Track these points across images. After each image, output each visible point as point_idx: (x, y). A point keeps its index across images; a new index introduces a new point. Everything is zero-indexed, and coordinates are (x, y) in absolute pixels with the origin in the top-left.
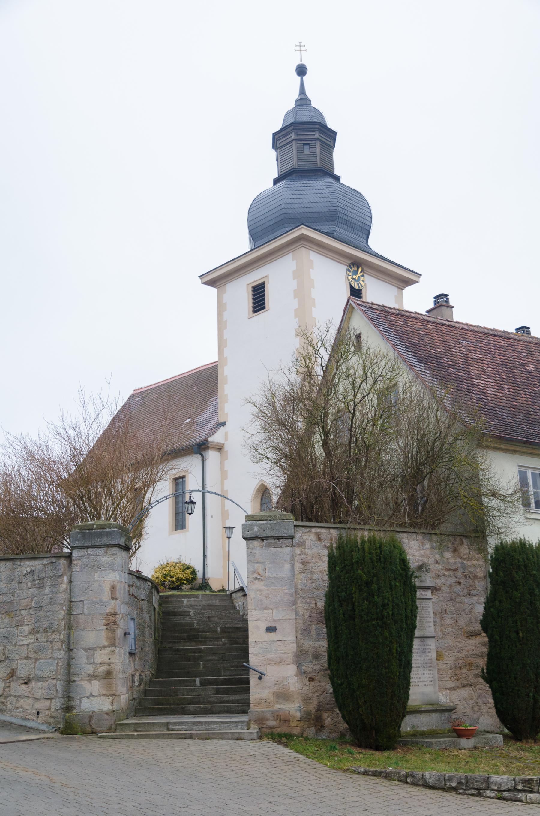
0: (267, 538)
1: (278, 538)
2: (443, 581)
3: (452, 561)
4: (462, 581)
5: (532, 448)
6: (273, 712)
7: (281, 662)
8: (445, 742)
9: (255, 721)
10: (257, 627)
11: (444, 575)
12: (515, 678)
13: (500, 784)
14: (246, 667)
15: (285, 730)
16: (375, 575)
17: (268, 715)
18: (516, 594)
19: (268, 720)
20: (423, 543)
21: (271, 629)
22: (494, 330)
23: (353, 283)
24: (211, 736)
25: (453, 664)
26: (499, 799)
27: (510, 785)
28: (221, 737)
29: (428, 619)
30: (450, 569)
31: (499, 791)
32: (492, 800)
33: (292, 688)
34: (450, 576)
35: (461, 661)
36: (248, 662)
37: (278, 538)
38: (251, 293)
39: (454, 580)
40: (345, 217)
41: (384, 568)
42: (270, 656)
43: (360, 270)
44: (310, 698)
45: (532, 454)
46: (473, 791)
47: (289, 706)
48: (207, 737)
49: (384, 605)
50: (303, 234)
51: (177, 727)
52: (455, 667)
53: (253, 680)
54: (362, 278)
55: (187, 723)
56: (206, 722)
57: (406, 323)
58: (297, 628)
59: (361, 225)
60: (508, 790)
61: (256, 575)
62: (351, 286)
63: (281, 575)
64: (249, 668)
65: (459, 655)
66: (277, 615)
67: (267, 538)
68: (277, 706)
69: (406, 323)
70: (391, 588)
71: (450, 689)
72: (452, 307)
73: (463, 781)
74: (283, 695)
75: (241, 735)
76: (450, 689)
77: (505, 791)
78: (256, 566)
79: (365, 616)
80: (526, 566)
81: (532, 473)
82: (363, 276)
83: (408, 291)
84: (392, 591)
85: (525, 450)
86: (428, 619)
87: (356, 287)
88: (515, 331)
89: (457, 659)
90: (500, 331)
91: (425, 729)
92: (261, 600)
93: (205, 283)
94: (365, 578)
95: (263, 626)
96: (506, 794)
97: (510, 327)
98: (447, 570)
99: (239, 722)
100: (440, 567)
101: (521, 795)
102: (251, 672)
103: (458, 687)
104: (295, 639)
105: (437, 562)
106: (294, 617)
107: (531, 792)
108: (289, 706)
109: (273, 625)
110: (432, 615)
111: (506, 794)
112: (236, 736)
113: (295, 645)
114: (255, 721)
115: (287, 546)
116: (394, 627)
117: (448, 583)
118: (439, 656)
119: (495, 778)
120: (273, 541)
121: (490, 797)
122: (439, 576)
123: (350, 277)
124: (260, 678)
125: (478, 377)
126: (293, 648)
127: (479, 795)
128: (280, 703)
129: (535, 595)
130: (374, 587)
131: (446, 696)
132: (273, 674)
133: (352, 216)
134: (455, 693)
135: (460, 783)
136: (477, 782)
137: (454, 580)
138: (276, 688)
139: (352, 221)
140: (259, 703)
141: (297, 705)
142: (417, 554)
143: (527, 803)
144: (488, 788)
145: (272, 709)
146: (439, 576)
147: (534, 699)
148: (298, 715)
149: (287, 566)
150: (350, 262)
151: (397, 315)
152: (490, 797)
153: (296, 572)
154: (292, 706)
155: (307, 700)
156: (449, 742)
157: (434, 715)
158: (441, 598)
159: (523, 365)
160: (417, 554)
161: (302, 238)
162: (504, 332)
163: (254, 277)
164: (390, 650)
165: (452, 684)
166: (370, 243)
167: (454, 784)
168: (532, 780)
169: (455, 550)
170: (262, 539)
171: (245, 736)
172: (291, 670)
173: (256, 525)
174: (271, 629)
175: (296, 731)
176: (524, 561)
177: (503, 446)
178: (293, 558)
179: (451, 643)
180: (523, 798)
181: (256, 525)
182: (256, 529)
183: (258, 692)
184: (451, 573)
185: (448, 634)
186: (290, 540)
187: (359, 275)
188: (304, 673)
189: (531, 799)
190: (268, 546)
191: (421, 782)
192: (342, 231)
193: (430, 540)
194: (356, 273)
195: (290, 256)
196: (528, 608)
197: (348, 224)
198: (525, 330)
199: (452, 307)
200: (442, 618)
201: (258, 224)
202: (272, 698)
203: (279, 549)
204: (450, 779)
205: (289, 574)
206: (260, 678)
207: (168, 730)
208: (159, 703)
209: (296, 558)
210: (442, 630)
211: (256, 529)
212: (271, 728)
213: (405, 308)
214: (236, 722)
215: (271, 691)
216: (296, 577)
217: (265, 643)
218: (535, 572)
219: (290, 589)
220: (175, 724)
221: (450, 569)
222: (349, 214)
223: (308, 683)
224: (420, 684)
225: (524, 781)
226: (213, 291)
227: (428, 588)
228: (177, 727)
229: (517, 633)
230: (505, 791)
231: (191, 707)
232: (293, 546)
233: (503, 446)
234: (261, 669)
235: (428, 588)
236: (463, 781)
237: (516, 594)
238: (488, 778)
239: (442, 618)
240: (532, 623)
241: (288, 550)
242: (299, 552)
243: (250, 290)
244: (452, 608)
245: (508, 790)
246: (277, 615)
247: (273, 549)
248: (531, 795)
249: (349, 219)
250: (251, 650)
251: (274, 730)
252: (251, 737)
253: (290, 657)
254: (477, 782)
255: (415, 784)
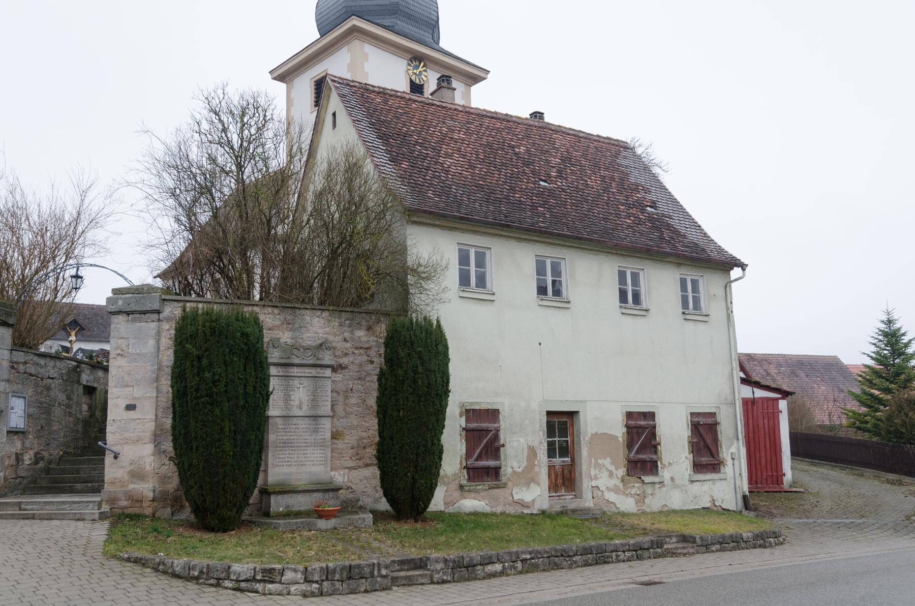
0: (132, 312)
1: (144, 313)
2: (351, 359)
3: (365, 339)
4: (375, 360)
5: (473, 226)
6: (125, 493)
7: (138, 441)
8: (297, 523)
9: (107, 501)
10: (117, 405)
11: (353, 353)
12: (395, 458)
13: (239, 574)
14: (102, 447)
15: (136, 510)
16: (206, 350)
17: (120, 495)
18: (400, 372)
19: (120, 500)
20: (329, 321)
21: (130, 407)
22: (496, 113)
23: (413, 78)
24: (53, 516)
25: (355, 444)
26: (235, 589)
27: (249, 574)
28: (61, 517)
29: (325, 398)
30: (361, 348)
31: (238, 581)
32: (229, 591)
33: (148, 468)
34: (360, 355)
35: (365, 441)
36: (104, 440)
37: (144, 313)
38: (313, 87)
39: (365, 358)
40: (407, 10)
41: (218, 342)
42: (127, 435)
43: (422, 64)
44: (169, 478)
45: (475, 232)
46: (212, 581)
47: (143, 486)
48: (50, 518)
49: (215, 382)
50: (354, 25)
51: (29, 507)
52: (359, 446)
53: (109, 459)
54: (424, 73)
55: (40, 503)
56: (58, 502)
57: (385, 102)
58: (157, 406)
59: (426, 19)
60: (247, 580)
61: (119, 351)
62: (411, 81)
63: (144, 351)
64: (105, 449)
65: (364, 434)
66: (138, 392)
67: (132, 312)
68: (132, 486)
69: (385, 102)
70: (225, 363)
71: (350, 468)
72: (455, 89)
73: (205, 570)
74: (137, 475)
75: (83, 516)
76: (350, 468)
77: (243, 581)
78: (120, 341)
79: (194, 393)
80: (412, 343)
81: (692, 280)
82: (425, 71)
83: (476, 89)
84: (226, 366)
85: (464, 227)
86: (325, 398)
87: (417, 82)
88: (529, 117)
89: (361, 439)
90: (501, 114)
91: (302, 509)
92: (123, 377)
93: (274, 79)
94: (196, 353)
95: (123, 403)
96: (243, 585)
97: (523, 112)
98: (357, 348)
99: (90, 502)
100: (349, 345)
101: (259, 587)
102: (107, 452)
103: (359, 467)
104: (154, 417)
105: (345, 340)
106: (155, 395)
107: (272, 582)
108: (143, 486)
109: (133, 403)
110: (329, 393)
111: (243, 585)
112: (78, 516)
113: (153, 424)
114: (107, 501)
115: (153, 321)
116: (227, 404)
117: (357, 361)
118: (335, 436)
119: (236, 567)
120: (138, 316)
121: (226, 588)
122: (346, 354)
123: (410, 72)
124: (116, 457)
125: (448, 155)
126: (151, 426)
127: (218, 585)
128: (135, 483)
129: (419, 373)
130: (205, 362)
131: (344, 475)
132: (129, 453)
133: (416, 9)
134: (355, 473)
135: (201, 572)
136: (217, 571)
137: (365, 358)
138: (132, 467)
139: (416, 15)
140: (113, 483)
141: (151, 485)
142: (320, 331)
143: (264, 594)
144: (228, 578)
145: (125, 489)
146: (346, 354)
147: (413, 478)
148: (151, 495)
149: (152, 342)
150: (410, 56)
151: (379, 93)
152: (226, 588)
153: (162, 348)
154: (147, 486)
155: (163, 479)
156: (302, 523)
157: (315, 494)
158: (347, 377)
159: (513, 147)
160: (320, 331)
161: (354, 30)
162: (507, 115)
163: (316, 72)
164: (222, 429)
165: (351, 464)
166: (444, 44)
167: (196, 574)
168: (274, 569)
169: (369, 328)
170: (128, 313)
171: (87, 517)
172: (149, 448)
173: (121, 298)
174: (130, 407)
175: (149, 511)
176: (411, 337)
177: (438, 223)
178: (159, 334)
179: (355, 423)
180: (260, 589)
181: (121, 298)
182: (120, 302)
183: (113, 471)
184: (362, 351)
185: (352, 413)
186: (156, 315)
187: (420, 69)
188: (164, 452)
189: (269, 590)
190: (134, 321)
191: (170, 571)
192: (405, 25)
193: (339, 317)
194: (417, 67)
195: (345, 49)
196: (410, 387)
197: (410, 17)
198: (537, 115)
199: (455, 89)
200: (346, 397)
201: (325, 18)
202: (126, 478)
203: (144, 324)
204: (194, 568)
205: (153, 350)
206: (116, 457)
207: (20, 509)
208: (55, 481)
209: (164, 334)
210: (345, 410)
211: (120, 302)
212: (123, 508)
213: (473, 105)
214: (88, 502)
215: (126, 470)
216: (161, 353)
217: (123, 422)
218: (419, 349)
219: (153, 365)
220: (28, 503)
221: (361, 348)
222: (412, 7)
223: (167, 462)
224: (307, 463)
225: (264, 571)
226: (282, 86)
227: (327, 366)
228: (29, 507)
229: (399, 411)
230: (243, 581)
231: (79, 486)
232: (159, 320)
233: (548, 240)
234: (116, 449)
235: (327, 366)
236: (205, 570)
237: (400, 372)
238: (229, 567)
239: (346, 397)
240: (413, 401)
241: (154, 325)
242: (167, 328)
243: (313, 84)
244: (360, 387)
245: (247, 580)
246: (138, 392)
247: (138, 324)
248: (270, 586)
249: (413, 13)
250: (109, 429)
251: (125, 511)
252: (92, 518)
253: (148, 435)
254: (217, 571)
255: (165, 572)
